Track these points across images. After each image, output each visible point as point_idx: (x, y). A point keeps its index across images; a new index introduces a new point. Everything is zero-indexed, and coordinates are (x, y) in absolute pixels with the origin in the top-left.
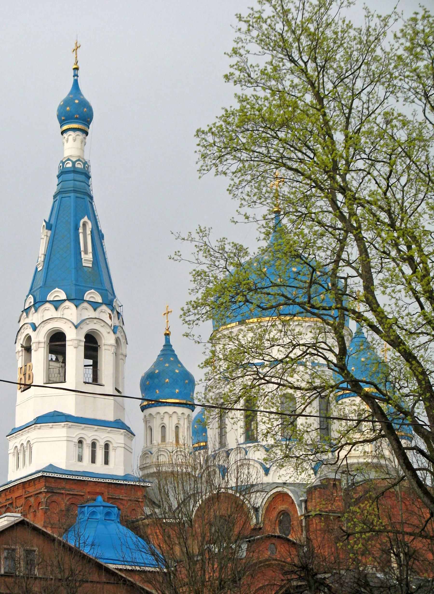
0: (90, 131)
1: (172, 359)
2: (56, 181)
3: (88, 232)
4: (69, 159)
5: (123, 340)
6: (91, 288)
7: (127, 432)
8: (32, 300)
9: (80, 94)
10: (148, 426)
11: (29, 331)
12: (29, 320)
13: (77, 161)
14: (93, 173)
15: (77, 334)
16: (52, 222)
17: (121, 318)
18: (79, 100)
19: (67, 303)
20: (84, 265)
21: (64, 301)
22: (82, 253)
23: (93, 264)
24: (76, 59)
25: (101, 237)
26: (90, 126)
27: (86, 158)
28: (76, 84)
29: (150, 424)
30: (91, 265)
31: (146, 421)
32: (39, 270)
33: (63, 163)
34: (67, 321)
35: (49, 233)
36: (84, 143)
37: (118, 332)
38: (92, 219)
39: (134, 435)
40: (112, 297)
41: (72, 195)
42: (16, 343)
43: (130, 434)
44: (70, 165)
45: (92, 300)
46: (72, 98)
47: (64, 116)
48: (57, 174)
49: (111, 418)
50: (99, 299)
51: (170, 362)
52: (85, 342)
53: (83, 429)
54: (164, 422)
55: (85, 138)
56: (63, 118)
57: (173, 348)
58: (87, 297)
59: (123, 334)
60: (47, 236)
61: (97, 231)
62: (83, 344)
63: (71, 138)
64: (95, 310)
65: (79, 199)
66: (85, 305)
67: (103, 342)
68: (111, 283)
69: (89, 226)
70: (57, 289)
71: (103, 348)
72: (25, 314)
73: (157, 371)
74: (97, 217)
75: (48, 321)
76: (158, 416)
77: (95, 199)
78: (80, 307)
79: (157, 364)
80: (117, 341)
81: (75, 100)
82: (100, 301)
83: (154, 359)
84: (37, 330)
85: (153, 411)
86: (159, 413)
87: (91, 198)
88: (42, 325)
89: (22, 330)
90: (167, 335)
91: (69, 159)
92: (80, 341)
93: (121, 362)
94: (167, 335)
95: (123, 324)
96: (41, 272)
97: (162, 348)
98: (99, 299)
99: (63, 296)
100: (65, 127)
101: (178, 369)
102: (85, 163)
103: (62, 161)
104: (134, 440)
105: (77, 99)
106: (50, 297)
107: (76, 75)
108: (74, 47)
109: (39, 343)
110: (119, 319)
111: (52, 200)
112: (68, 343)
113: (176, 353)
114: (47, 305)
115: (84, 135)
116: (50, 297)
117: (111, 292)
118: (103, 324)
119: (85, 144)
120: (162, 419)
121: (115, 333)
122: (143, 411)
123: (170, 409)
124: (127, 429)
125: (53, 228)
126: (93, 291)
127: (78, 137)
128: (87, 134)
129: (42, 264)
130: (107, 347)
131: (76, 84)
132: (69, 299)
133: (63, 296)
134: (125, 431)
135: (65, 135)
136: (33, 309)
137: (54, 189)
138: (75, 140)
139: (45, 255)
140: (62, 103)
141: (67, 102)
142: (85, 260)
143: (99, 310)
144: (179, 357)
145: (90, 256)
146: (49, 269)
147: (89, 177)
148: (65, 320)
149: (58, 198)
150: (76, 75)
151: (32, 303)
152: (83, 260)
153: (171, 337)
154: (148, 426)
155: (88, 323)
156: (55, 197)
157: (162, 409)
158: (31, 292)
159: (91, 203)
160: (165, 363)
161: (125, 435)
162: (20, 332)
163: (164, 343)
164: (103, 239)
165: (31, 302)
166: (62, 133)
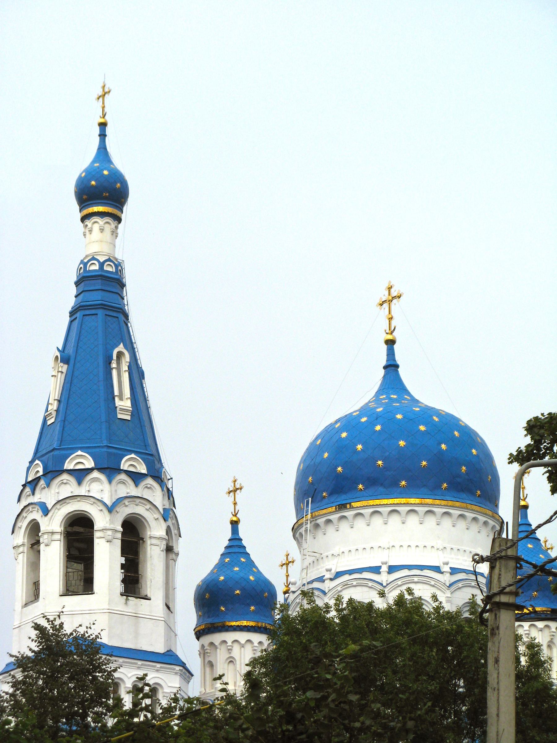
0: (123, 217)
1: (243, 560)
2: (73, 291)
3: (125, 367)
4: (93, 259)
5: (174, 531)
6: (131, 452)
7: (184, 670)
8: (41, 470)
9: (110, 161)
10: (206, 662)
11: (37, 515)
12: (36, 499)
13: (106, 261)
14: (129, 278)
15: (112, 522)
16: (70, 350)
17: (171, 499)
18: (109, 171)
19: (96, 474)
20: (120, 416)
21: (90, 470)
22: (117, 399)
23: (132, 416)
24: (103, 110)
25: (141, 375)
26: (125, 209)
27: (119, 255)
28: (103, 149)
29: (211, 659)
30: (129, 418)
31: (203, 653)
32: (49, 422)
33: (85, 264)
34: (96, 501)
35: (65, 368)
36: (114, 233)
37: (169, 520)
38: (129, 349)
39: (192, 675)
40: (159, 466)
41: (100, 312)
42: (103, 125)
43: (188, 674)
44: (96, 267)
45: (132, 469)
46: (98, 167)
47: (86, 194)
48: (75, 279)
49: (160, 649)
50: (142, 469)
51: (240, 564)
52: (123, 534)
53: (157, 671)
54: (233, 655)
55: (117, 227)
56: (85, 197)
57: (244, 543)
58: (125, 465)
59: (174, 521)
60: (62, 372)
61: (135, 366)
62: (119, 535)
63: (96, 227)
64: (137, 485)
65: (109, 318)
66: (123, 476)
67: (149, 533)
68: (156, 445)
69: (127, 357)
70: (79, 453)
71: (149, 542)
72: (28, 490)
73: (222, 578)
74: (135, 345)
75: (67, 501)
76: (223, 647)
77: (130, 318)
78: (114, 482)
79: (221, 566)
80: (168, 531)
81: (103, 170)
82: (144, 471)
83: (215, 559)
84: (50, 514)
85: (217, 638)
86: (225, 642)
87: (126, 316)
88: (58, 506)
89: (24, 514)
90: (390, 343)
91: (93, 259)
92: (116, 531)
93: (171, 562)
94: (390, 343)
95: (174, 506)
96: (53, 426)
97: (226, 543)
98: (142, 469)
99: (89, 463)
100: (86, 212)
101: (253, 576)
102: (118, 265)
103: (82, 262)
104: (192, 681)
105: (105, 169)
106: (69, 465)
107: (103, 136)
108: (100, 93)
109: (53, 533)
110: (169, 499)
111: (67, 319)
112: (97, 535)
113: (248, 550)
114: (65, 477)
115: (113, 224)
116: (69, 465)
117: (157, 457)
118: (148, 506)
119: (117, 236)
120: (230, 650)
121: (165, 520)
122: (198, 639)
123: (242, 637)
124: (183, 665)
125: (72, 362)
126: (133, 456)
127: (107, 225)
128: (119, 220)
129: (54, 414)
130: (154, 541)
131: (103, 149)
132: (100, 469)
133: (89, 463)
134: (181, 668)
135: (89, 223)
136: (42, 482)
137: (70, 302)
138: (102, 230)
139: (59, 401)
140: (83, 175)
141: (90, 173)
142: (121, 409)
143: (143, 484)
144: (252, 557)
145: (127, 404)
146: (66, 423)
147: (123, 285)
148: (92, 500)
149: (78, 315)
150: (103, 136)
151: (41, 473)
152: (118, 409)
153: (240, 527)
154: (206, 662)
155: (127, 503)
156: (72, 313)
157: (230, 637)
158: (37, 455)
159: (127, 325)
160: (234, 567)
161: (181, 675)
162: (21, 517)
163: (229, 535)
164: (144, 378)
165: (38, 472)
166: (83, 219)
